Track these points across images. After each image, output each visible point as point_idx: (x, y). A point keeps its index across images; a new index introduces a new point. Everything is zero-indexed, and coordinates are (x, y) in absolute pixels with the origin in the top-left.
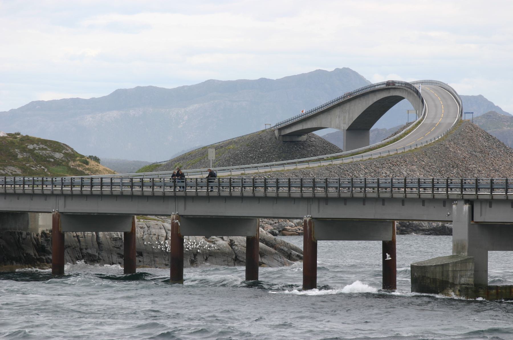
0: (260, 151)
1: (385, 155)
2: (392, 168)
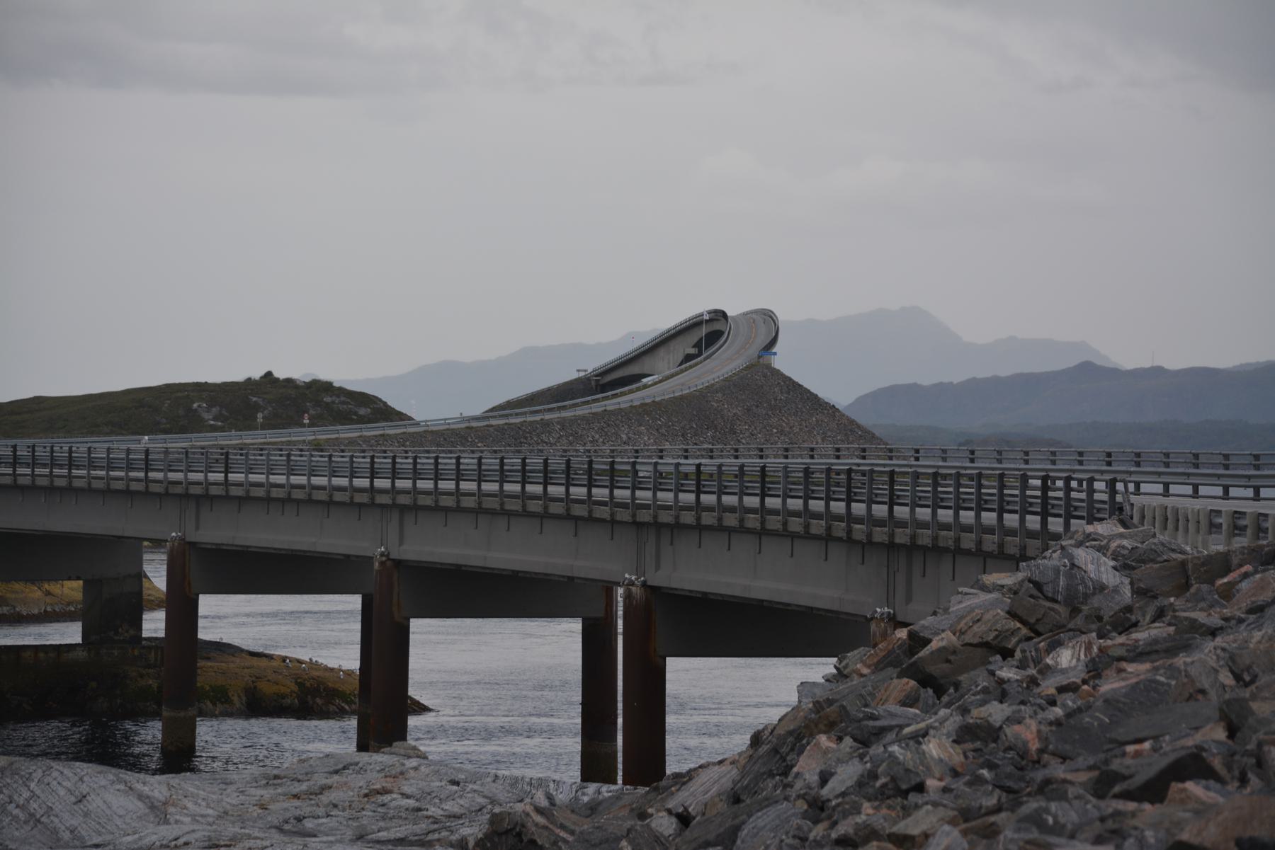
2: (606, 430)
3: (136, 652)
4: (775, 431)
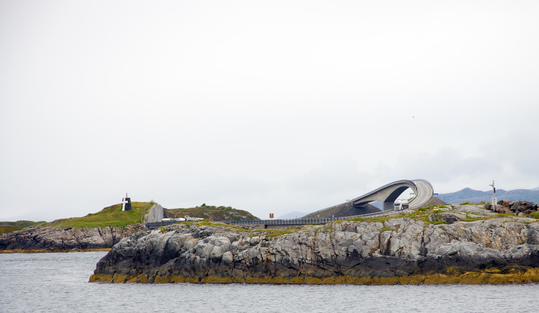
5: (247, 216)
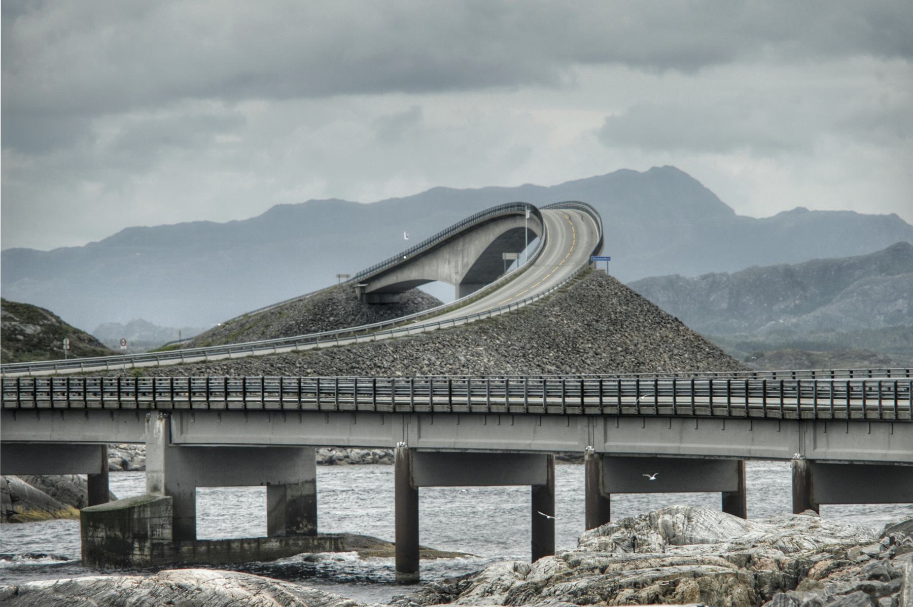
0: (329, 321)
1: (432, 329)
2: (442, 351)
3: (316, 543)
4: (620, 349)
5: (41, 326)
